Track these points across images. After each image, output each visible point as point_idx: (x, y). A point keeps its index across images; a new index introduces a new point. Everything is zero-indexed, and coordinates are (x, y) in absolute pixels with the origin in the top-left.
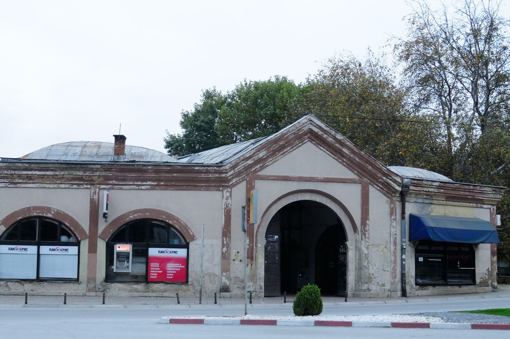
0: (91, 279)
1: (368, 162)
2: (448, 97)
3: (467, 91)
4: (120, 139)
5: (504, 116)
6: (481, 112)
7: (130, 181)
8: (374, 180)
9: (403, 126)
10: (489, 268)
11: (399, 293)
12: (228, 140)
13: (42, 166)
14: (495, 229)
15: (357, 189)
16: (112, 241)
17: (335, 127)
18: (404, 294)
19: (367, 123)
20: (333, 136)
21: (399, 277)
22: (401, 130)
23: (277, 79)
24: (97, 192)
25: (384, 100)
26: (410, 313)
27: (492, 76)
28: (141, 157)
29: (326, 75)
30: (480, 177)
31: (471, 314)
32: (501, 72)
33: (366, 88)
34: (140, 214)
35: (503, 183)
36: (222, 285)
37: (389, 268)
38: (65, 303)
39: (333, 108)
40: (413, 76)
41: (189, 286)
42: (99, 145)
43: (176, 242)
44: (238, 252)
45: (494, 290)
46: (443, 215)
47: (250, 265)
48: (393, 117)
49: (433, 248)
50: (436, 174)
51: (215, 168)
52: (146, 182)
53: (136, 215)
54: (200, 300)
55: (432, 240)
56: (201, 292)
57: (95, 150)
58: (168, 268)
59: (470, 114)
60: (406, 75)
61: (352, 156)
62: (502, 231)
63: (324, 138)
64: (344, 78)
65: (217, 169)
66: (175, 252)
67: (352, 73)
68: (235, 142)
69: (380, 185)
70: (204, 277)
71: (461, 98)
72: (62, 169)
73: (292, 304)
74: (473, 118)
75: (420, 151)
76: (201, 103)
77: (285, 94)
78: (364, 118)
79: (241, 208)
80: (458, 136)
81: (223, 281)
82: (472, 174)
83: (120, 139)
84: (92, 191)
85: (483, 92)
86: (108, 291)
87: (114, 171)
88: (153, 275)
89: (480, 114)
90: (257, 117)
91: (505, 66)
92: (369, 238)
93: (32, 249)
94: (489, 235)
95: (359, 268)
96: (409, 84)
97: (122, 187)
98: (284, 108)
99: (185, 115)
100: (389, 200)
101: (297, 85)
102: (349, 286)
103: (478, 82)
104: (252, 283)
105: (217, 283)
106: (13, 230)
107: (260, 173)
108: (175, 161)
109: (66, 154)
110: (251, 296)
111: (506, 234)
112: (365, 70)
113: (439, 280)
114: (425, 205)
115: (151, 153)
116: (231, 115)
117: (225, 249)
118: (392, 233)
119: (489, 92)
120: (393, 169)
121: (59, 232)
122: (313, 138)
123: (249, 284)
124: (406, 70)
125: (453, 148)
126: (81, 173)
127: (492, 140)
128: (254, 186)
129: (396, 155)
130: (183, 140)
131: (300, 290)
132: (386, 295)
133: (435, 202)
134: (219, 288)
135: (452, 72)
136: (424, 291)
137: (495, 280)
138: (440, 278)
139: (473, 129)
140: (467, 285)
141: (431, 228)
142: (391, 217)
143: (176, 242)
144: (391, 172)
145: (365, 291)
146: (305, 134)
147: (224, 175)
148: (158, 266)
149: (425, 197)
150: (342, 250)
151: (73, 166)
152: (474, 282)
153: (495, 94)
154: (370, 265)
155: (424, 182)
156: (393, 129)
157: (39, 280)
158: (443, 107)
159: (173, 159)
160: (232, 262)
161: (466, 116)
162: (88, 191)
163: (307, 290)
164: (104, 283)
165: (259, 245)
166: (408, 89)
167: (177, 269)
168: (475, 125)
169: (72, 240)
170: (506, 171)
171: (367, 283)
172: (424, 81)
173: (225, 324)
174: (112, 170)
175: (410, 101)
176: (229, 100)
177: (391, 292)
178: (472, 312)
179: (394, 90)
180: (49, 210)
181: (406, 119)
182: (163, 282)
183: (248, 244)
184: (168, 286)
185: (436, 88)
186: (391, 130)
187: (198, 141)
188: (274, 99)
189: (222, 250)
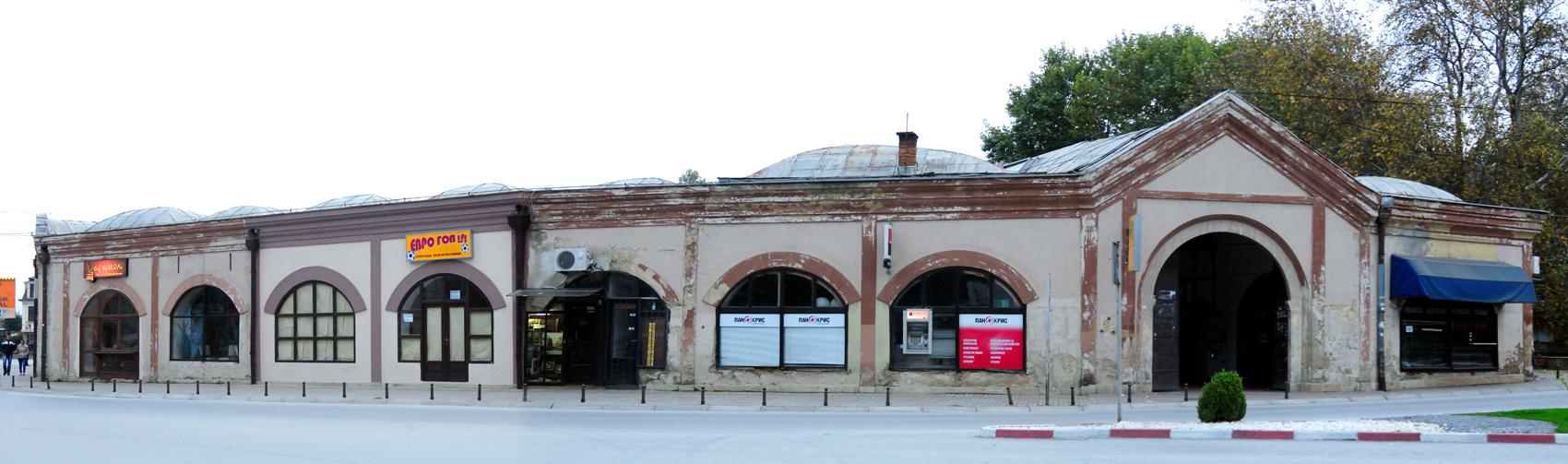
0: (867, 365)
1: (1323, 169)
2: (1457, 63)
3: (1488, 53)
4: (908, 139)
5: (1548, 95)
6: (1511, 87)
7: (925, 206)
8: (1333, 198)
9: (1383, 111)
10: (1519, 344)
11: (1374, 385)
12: (1095, 133)
13: (784, 188)
14: (1530, 280)
15: (1306, 213)
16: (899, 304)
17: (1272, 111)
18: (1382, 386)
19: (1324, 105)
20: (1265, 125)
21: (1373, 358)
22: (1379, 116)
23: (1177, 31)
24: (873, 225)
25: (1352, 66)
26: (1389, 416)
27: (1530, 29)
28: (943, 166)
29: (1257, 24)
30: (1507, 194)
31: (1488, 419)
32: (1545, 22)
33: (1323, 46)
34: (944, 260)
35: (1544, 205)
37: (1357, 344)
38: (826, 404)
39: (1268, 80)
40: (1401, 27)
42: (873, 151)
43: (1005, 304)
44: (1109, 319)
45: (1528, 378)
46: (1446, 256)
47: (1128, 339)
48: (1367, 95)
49: (1430, 311)
50: (1435, 189)
51: (1067, 179)
54: (1047, 399)
55: (1427, 298)
56: (1047, 387)
57: (867, 159)
59: (1493, 90)
60: (1389, 25)
61: (1297, 159)
62: (1542, 284)
63: (1252, 130)
64: (1287, 29)
65: (1071, 181)
66: (1003, 321)
67: (1300, 22)
68: (1106, 136)
69: (1343, 208)
70: (1052, 360)
71: (1480, 65)
72: (815, 192)
73: (1196, 404)
74: (1498, 98)
75: (1409, 152)
76: (1041, 72)
77: (1190, 55)
78: (1319, 97)
79: (1111, 245)
80: (1473, 127)
81: (1086, 367)
82: (1493, 190)
83: (908, 139)
84: (866, 225)
85: (1516, 55)
86: (894, 384)
87: (899, 192)
88: (968, 359)
89: (1508, 91)
90: (1142, 95)
91: (1552, 11)
92: (1324, 295)
93: (772, 320)
94: (1520, 289)
95: (1309, 343)
96: (1394, 40)
97: (912, 216)
98: (1188, 79)
99: (1014, 94)
100: (1358, 232)
101: (1209, 41)
102: (1292, 373)
103: (1508, 38)
104: (1131, 370)
105: (1075, 371)
106: (740, 291)
107: (1145, 188)
108: (1000, 171)
109: (821, 168)
110: (1129, 390)
111: (1549, 288)
112: (1323, 17)
113: (1438, 363)
114: (1417, 240)
115: (959, 160)
116: (1100, 91)
117: (1086, 315)
118: (1362, 286)
119: (1524, 53)
120: (1366, 181)
121: (813, 291)
122: (1233, 130)
123: (1126, 370)
124: (1389, 17)
125: (1465, 146)
126: (846, 197)
127: (1527, 134)
128: (1136, 209)
129: (1371, 158)
130: (1012, 136)
131: (1209, 380)
132: (1352, 388)
133: (1432, 235)
134: (1079, 379)
135: (1465, 21)
136: (1414, 381)
137: (1530, 363)
138: (1440, 360)
139: (1498, 115)
140: (1484, 370)
141: (1427, 277)
142: (1361, 260)
143: (1005, 304)
144: (1362, 185)
145: (1318, 380)
146: (1221, 123)
147: (1081, 192)
149: (1417, 227)
150: (1280, 315)
151: (833, 186)
152: (1495, 367)
153: (1534, 58)
154: (1326, 339)
155: (1416, 203)
156: (1367, 115)
157: (784, 367)
158: (1449, 79)
159: (996, 169)
160: (1099, 334)
161: (1487, 94)
162: (859, 224)
163: (1222, 380)
164: (888, 372)
165: (1144, 307)
166: (1392, 49)
167: (1007, 349)
168: (1501, 109)
169: (834, 304)
170: (1550, 185)
171: (1321, 368)
172: (1419, 37)
173: (1087, 438)
174: (897, 189)
175: (1395, 68)
176: (1097, 66)
177: (1360, 382)
178: (1489, 415)
179: (1369, 50)
180: (796, 257)
181: (1388, 98)
182: (984, 370)
183: (1125, 306)
184: (993, 377)
185: (1439, 47)
186: (1364, 117)
187: (1038, 137)
188: (1171, 64)
189: (1082, 316)
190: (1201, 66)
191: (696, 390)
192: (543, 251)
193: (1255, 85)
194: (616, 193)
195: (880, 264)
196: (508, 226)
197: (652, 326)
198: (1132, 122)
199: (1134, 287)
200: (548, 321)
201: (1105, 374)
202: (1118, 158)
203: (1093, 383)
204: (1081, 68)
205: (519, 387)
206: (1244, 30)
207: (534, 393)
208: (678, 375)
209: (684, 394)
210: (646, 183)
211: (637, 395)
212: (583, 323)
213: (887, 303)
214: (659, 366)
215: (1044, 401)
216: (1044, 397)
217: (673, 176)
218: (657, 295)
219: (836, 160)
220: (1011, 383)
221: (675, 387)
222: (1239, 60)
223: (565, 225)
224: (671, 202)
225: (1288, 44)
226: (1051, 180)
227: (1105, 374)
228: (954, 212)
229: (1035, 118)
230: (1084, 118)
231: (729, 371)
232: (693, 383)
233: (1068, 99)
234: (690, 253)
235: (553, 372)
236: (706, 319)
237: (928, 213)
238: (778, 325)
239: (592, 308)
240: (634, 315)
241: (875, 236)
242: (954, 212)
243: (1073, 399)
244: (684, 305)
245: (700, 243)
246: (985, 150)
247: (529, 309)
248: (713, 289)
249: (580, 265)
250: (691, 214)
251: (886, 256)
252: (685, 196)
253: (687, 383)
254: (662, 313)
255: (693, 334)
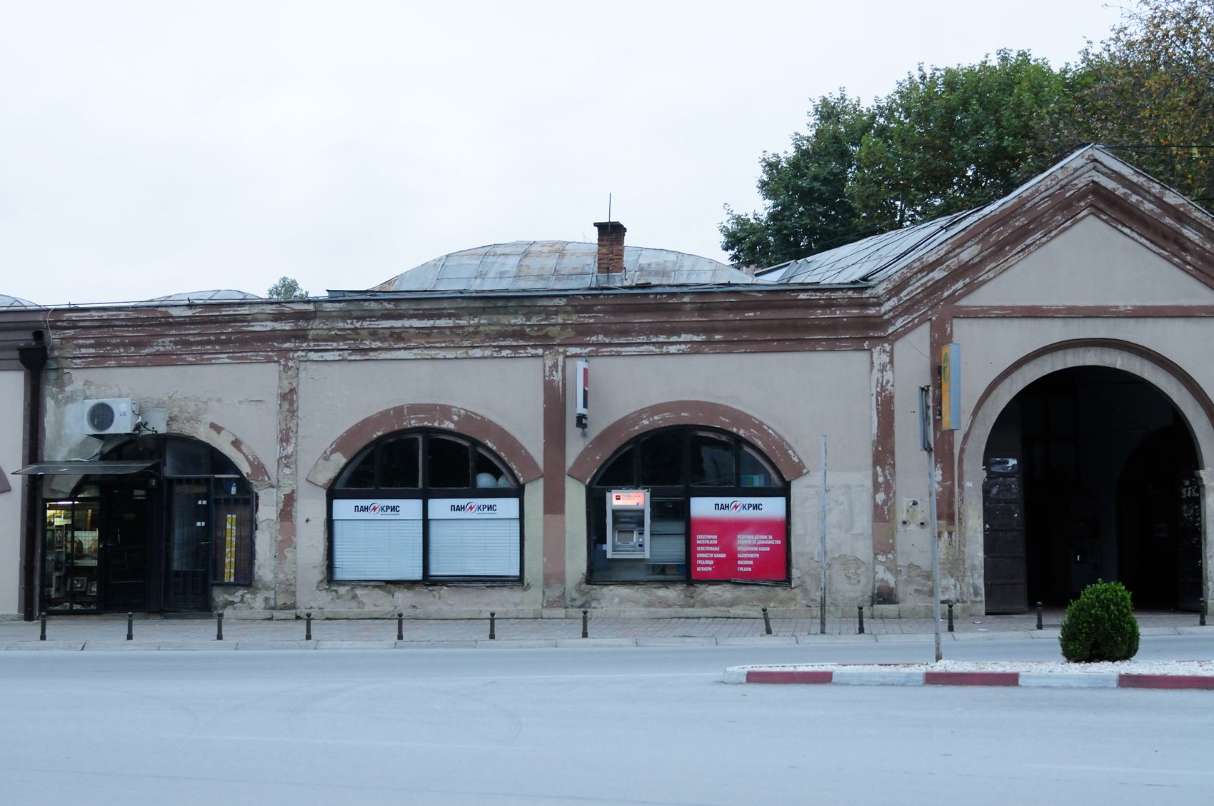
0: (553, 577)
4: (611, 233)
7: (639, 333)
12: (883, 222)
13: (426, 306)
17: (1161, 173)
20: (1154, 196)
24: (560, 363)
28: (664, 273)
34: (667, 415)
36: (877, 585)
38: (492, 636)
41: (793, 590)
42: (560, 250)
47: (946, 535)
51: (850, 293)
52: (679, 337)
53: (656, 418)
54: (823, 624)
56: (823, 606)
57: (551, 263)
58: (740, 545)
63: (1131, 205)
64: (1184, 43)
65: (856, 295)
66: (756, 507)
67: (1204, 30)
70: (829, 565)
72: (474, 313)
73: (1057, 633)
76: (810, 133)
77: (1026, 95)
79: (917, 392)
83: (611, 233)
84: (549, 363)
87: (597, 312)
88: (704, 565)
90: (954, 161)
93: (410, 508)
97: (619, 349)
98: (1025, 132)
99: (770, 165)
102: (1210, 584)
104: (952, 581)
105: (863, 581)
107: (964, 302)
108: (749, 280)
109: (481, 275)
110: (950, 612)
115: (688, 264)
116: (888, 158)
117: (881, 497)
121: (471, 464)
122: (1101, 205)
123: (944, 582)
126: (519, 320)
128: (951, 335)
130: (767, 227)
131: (1077, 596)
134: (870, 594)
143: (758, 481)
146: (1081, 196)
147: (872, 311)
148: (716, 542)
150: (1187, 493)
151: (500, 304)
157: (428, 581)
159: (744, 277)
160: (900, 527)
162: (539, 362)
163: (1097, 597)
164: (584, 586)
165: (968, 484)
169: (503, 483)
180: (446, 411)
182: (728, 582)
184: (741, 592)
189: (875, 499)
190: (1045, 111)
191: (298, 618)
192: (65, 404)
193: (1137, 136)
194: (175, 312)
195: (571, 422)
196: (18, 363)
197: (231, 521)
198: (938, 202)
199: (952, 454)
200: (76, 513)
201: (911, 588)
202: (920, 259)
203: (895, 603)
204: (870, 126)
205: (29, 616)
206: (1113, 49)
207: (55, 627)
208: (271, 594)
209: (282, 625)
210: (219, 298)
211: (210, 627)
212: (130, 516)
213: (580, 480)
214: (242, 582)
215: (818, 628)
216: (819, 621)
217: (260, 288)
218: (238, 471)
219: (503, 264)
220: (769, 599)
221: (267, 614)
222: (1104, 97)
223: (99, 361)
224: (257, 327)
225: (1184, 65)
226: (826, 295)
227: (911, 588)
228: (680, 343)
229: (802, 201)
230: (875, 201)
231: (347, 588)
232: (293, 607)
233: (851, 172)
234: (286, 406)
235: (84, 594)
236: (311, 508)
237: (642, 344)
238: (420, 516)
239: (142, 492)
240: (205, 502)
241: (564, 379)
242: (680, 343)
243: (861, 623)
244: (278, 487)
245: (301, 390)
246: (726, 249)
247: (47, 495)
248: (322, 461)
249: (122, 425)
250: (287, 345)
251: (581, 410)
252: (278, 317)
253: (285, 607)
254: (246, 499)
255: (293, 531)
